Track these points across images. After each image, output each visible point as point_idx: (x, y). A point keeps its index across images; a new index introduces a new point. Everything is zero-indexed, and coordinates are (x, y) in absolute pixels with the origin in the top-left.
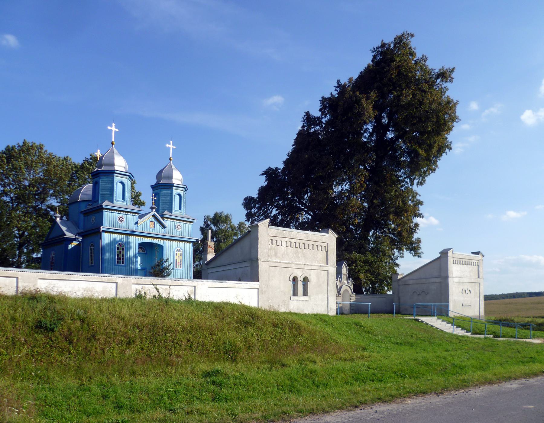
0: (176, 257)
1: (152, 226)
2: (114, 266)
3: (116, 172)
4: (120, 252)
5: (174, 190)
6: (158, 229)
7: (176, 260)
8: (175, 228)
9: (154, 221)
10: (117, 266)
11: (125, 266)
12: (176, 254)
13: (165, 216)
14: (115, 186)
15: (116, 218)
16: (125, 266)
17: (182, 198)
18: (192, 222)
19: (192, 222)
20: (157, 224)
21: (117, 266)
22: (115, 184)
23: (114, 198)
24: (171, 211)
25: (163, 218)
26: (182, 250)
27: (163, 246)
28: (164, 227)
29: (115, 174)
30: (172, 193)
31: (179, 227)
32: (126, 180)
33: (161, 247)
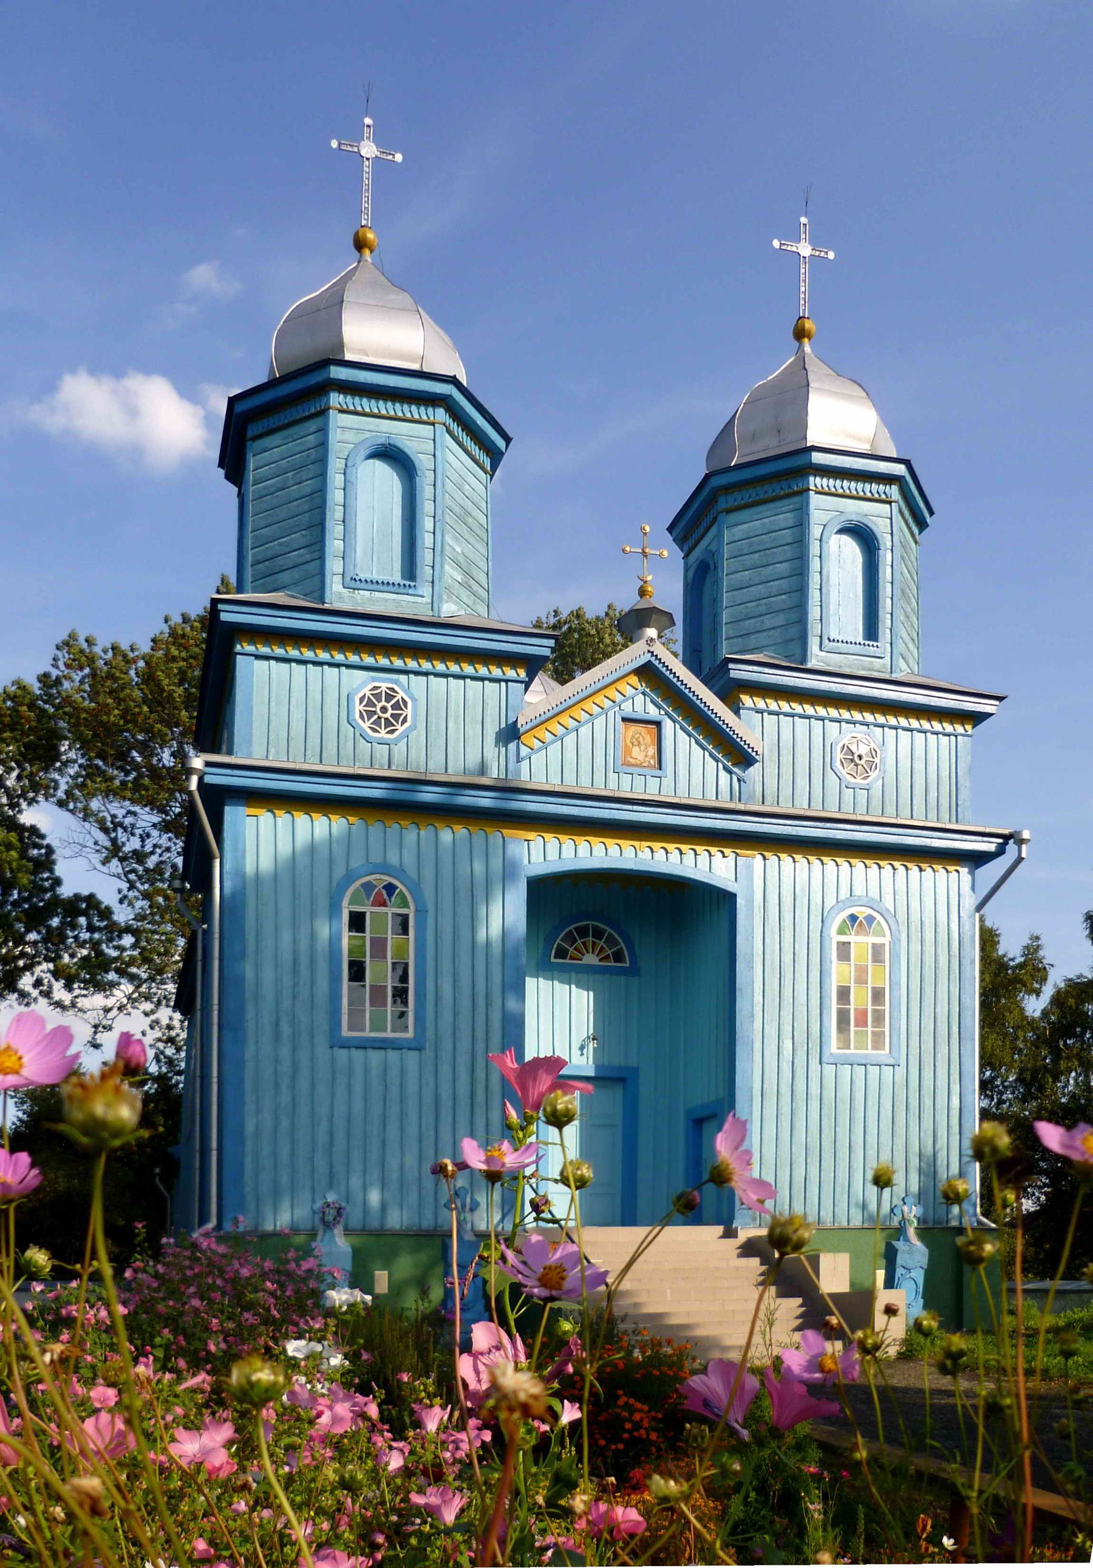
0: (838, 973)
1: (643, 753)
2: (322, 1050)
3: (817, 458)
4: (379, 946)
5: (815, 500)
6: (692, 772)
7: (844, 994)
8: (828, 764)
9: (653, 712)
10: (346, 1045)
11: (417, 1046)
12: (844, 951)
13: (738, 672)
14: (336, 479)
15: (827, 749)
16: (417, 1046)
17: (886, 557)
18: (976, 718)
19: (976, 718)
20: (677, 737)
21: (346, 1045)
22: (335, 465)
23: (334, 565)
24: (794, 648)
25: (732, 693)
26: (416, 889)
27: (732, 897)
28: (739, 756)
29: (336, 399)
30: (801, 524)
31: (387, 712)
32: (882, 517)
33: (719, 903)
